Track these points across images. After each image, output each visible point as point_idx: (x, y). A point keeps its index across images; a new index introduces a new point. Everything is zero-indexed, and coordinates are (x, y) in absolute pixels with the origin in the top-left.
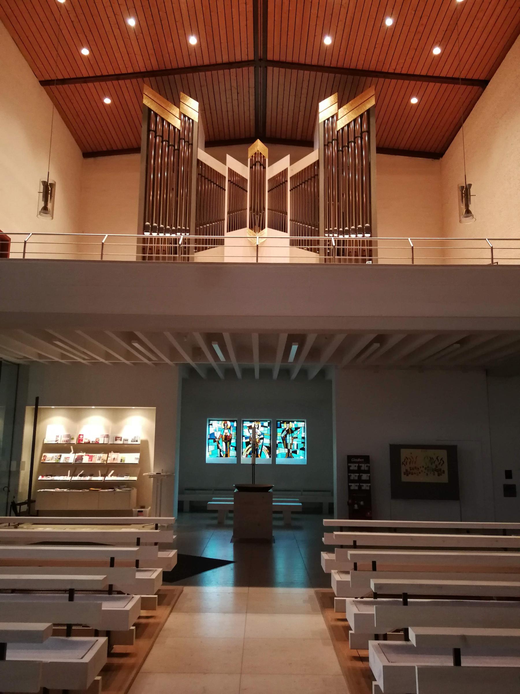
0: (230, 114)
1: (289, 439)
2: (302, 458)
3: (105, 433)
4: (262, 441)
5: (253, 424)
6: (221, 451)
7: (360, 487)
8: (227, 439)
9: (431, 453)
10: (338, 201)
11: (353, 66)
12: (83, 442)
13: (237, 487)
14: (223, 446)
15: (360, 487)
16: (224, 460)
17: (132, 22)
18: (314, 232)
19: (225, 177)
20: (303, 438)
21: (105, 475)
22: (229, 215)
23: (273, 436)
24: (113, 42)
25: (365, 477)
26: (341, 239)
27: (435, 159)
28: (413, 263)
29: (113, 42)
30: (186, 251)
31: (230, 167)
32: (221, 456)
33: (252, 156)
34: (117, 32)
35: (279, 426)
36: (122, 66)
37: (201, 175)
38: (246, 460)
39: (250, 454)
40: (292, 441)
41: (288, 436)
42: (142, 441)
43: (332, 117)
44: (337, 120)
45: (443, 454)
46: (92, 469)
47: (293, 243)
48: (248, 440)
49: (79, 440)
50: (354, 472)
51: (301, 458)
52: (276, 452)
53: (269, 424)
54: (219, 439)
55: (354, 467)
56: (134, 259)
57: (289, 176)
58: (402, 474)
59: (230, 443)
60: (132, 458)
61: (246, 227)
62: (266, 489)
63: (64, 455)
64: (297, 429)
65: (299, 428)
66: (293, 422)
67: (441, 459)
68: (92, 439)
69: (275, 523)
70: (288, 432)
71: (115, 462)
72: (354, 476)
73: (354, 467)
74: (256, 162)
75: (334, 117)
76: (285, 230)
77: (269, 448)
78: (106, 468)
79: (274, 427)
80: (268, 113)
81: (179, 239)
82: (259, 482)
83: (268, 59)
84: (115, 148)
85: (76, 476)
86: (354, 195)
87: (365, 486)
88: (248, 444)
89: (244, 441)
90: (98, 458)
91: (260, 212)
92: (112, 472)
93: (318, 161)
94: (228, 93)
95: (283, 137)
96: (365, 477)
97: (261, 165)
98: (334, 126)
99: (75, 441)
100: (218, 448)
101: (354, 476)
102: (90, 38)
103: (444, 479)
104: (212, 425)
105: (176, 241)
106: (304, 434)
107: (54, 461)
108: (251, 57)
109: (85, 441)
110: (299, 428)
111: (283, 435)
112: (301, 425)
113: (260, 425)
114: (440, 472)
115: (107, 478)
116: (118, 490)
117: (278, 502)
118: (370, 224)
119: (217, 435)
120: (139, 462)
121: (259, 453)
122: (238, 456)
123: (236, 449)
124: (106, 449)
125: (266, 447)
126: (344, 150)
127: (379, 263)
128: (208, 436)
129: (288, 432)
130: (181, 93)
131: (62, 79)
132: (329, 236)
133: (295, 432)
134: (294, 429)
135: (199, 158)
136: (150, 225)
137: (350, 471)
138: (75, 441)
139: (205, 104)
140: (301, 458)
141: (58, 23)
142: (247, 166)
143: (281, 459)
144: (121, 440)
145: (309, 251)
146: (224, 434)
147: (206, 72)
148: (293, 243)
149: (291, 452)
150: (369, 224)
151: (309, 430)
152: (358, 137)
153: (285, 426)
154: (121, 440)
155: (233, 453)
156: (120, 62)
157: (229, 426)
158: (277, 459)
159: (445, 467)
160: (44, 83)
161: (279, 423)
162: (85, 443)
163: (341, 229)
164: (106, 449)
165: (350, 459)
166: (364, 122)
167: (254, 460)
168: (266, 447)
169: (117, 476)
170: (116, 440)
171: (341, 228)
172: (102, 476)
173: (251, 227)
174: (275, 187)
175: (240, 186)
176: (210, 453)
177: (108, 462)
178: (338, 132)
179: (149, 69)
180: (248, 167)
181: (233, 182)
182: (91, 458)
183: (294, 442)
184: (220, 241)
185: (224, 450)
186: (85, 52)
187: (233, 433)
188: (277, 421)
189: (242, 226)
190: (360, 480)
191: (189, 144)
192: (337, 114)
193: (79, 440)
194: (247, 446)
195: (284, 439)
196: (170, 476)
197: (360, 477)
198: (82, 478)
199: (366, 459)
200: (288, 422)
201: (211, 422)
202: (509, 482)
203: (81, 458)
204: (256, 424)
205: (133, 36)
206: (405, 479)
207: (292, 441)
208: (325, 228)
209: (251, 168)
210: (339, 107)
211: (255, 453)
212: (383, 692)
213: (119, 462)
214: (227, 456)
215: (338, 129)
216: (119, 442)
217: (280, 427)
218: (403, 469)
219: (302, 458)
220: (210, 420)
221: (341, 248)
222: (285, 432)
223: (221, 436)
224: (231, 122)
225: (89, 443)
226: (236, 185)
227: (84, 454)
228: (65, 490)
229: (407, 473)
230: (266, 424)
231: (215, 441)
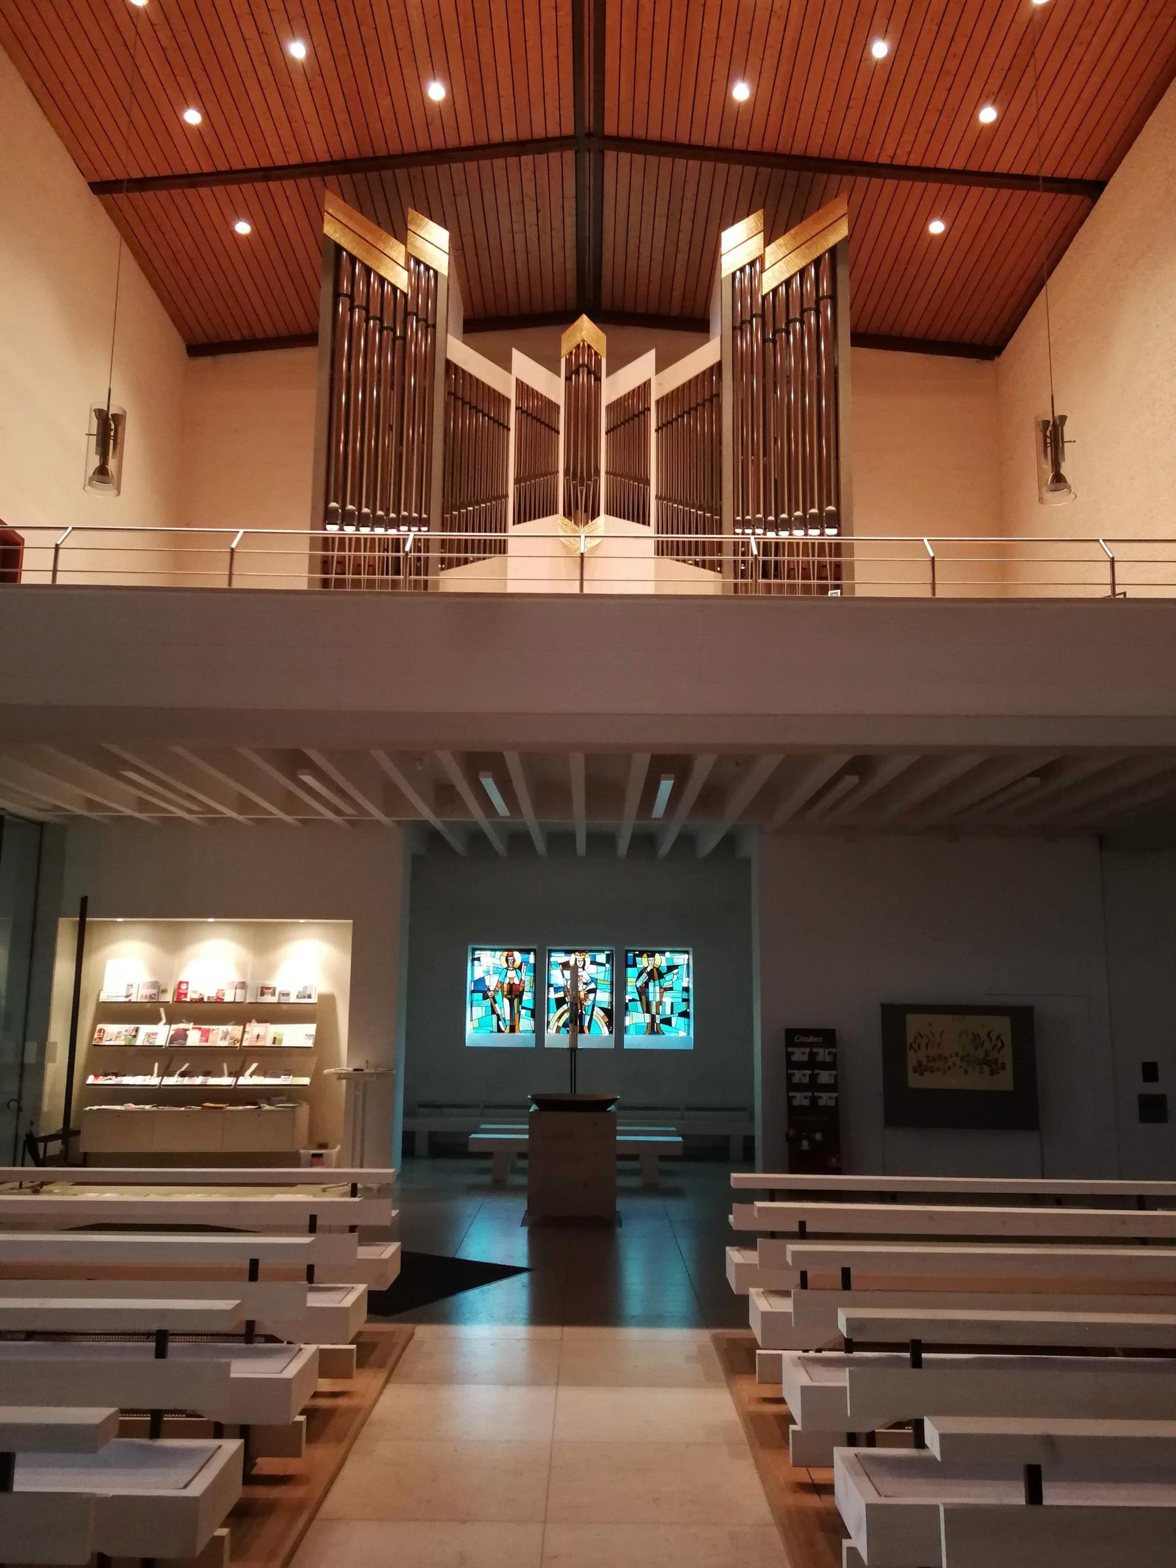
0: (521, 257)
1: (654, 991)
2: (682, 1034)
3: (237, 979)
4: (591, 996)
5: (571, 959)
6: (499, 1019)
7: (814, 1100)
8: (514, 993)
9: (975, 1023)
10: (765, 455)
11: (798, 149)
12: (188, 999)
13: (535, 1100)
14: (504, 1007)
15: (814, 1100)
16: (506, 1040)
17: (298, 50)
18: (710, 523)
19: (509, 401)
20: (686, 989)
21: (237, 1074)
22: (518, 486)
23: (618, 986)
24: (256, 95)
25: (824, 1077)
26: (771, 540)
27: (983, 359)
28: (934, 594)
29: (256, 95)
30: (422, 566)
31: (520, 378)
32: (499, 1030)
33: (571, 353)
34: (264, 71)
35: (630, 962)
36: (275, 150)
37: (455, 394)
38: (557, 1039)
39: (565, 1025)
40: (661, 997)
41: (651, 984)
42: (321, 997)
43: (752, 264)
44: (763, 270)
45: (1002, 1026)
46: (207, 1059)
47: (662, 549)
48: (561, 995)
49: (179, 994)
50: (800, 1066)
51: (680, 1034)
52: (623, 1021)
53: (609, 958)
54: (495, 991)
55: (799, 1055)
56: (303, 585)
57: (654, 397)
58: (910, 1071)
59: (520, 1002)
60: (297, 1035)
61: (556, 512)
62: (601, 1106)
63: (145, 1029)
64: (671, 968)
65: (676, 967)
66: (662, 953)
67: (998, 1037)
68: (209, 993)
69: (622, 1181)
70: (651, 975)
71: (259, 1044)
72: (802, 1076)
73: (799, 1055)
74: (579, 366)
76: (644, 520)
77: (608, 1012)
78: (239, 1058)
79: (620, 965)
80: (607, 254)
81: (405, 541)
82: (586, 1090)
83: (607, 133)
84: (260, 335)
85: (171, 1074)
86: (800, 442)
87: (825, 1099)
88: (560, 1002)
89: (553, 995)
90: (221, 1035)
91: (589, 479)
92: (254, 1066)
93: (719, 364)
94: (517, 209)
95: (641, 310)
96: (824, 1077)
97: (589, 373)
98: (755, 285)
99: (169, 997)
100: (493, 1011)
101: (802, 1076)
102: (204, 85)
103: (1005, 1081)
104: (478, 959)
105: (397, 544)
106: (687, 981)
107: (121, 1042)
108: (568, 129)
109: (191, 995)
111: (639, 984)
112: (681, 959)
113: (588, 960)
114: (995, 1067)
115: (243, 1081)
116: (267, 1107)
117: (629, 1135)
118: (838, 506)
119: (492, 982)
120: (315, 1043)
122: (539, 1031)
123: (533, 1016)
124: (240, 1014)
125: (602, 1009)
126: (777, 338)
127: (858, 594)
128: (470, 986)
129: (651, 975)
130: (410, 210)
131: (141, 179)
132: (743, 533)
133: (668, 977)
134: (664, 970)
135: (449, 357)
136: (340, 508)
137: (791, 1065)
138: (169, 997)
140: (680, 1034)
141: (132, 51)
142: (559, 375)
143: (636, 1038)
144: (273, 994)
145: (698, 566)
146: (507, 981)
147: (466, 164)
148: (662, 549)
149: (658, 1021)
150: (835, 507)
151: (699, 972)
152: (810, 309)
153: (643, 962)
154: (273, 994)
155: (526, 1023)
156: (272, 140)
157: (517, 963)
158: (625, 1036)
159: (1007, 1056)
160: (100, 188)
161: (630, 955)
162: (192, 1001)
164: (240, 1014)
165: (792, 1036)
166: (823, 276)
167: (574, 1040)
168: (602, 1009)
169: (265, 1075)
170: (262, 994)
171: (771, 515)
172: (230, 1075)
173: (568, 514)
174: (623, 423)
175: (542, 420)
176: (476, 1023)
177: (245, 1044)
178: (764, 298)
179: (338, 155)
180: (560, 376)
181: (526, 412)
182: (205, 1034)
183: (664, 1000)
184: (498, 543)
185: (508, 1017)
186: (193, 117)
187: (527, 977)
188: (628, 951)
189: (548, 510)
190: (813, 1085)
192: (761, 258)
193: (179, 994)
194: (558, 1007)
195: (643, 991)
196: (385, 1076)
197: (813, 1077)
198: (186, 1081)
199: (828, 1037)
200: (652, 954)
201: (477, 954)
202: (1152, 1089)
203: (183, 1035)
204: (580, 958)
205: (300, 82)
206: (915, 1081)
207: (661, 997)
208: (736, 514)
209: (568, 379)
211: (576, 1022)
212: (866, 1563)
213: (269, 1043)
214: (513, 1029)
215: (765, 291)
216: (268, 999)
217: (634, 965)
218: (912, 1059)
219: (682, 1034)
220: (474, 950)
221: (771, 561)
222: (644, 977)
223: (501, 984)
224: (522, 275)
225: (201, 1000)
226: (534, 418)
227: (191, 1025)
228: (147, 1107)
229: (920, 1069)
230: (601, 958)
231: (485, 997)
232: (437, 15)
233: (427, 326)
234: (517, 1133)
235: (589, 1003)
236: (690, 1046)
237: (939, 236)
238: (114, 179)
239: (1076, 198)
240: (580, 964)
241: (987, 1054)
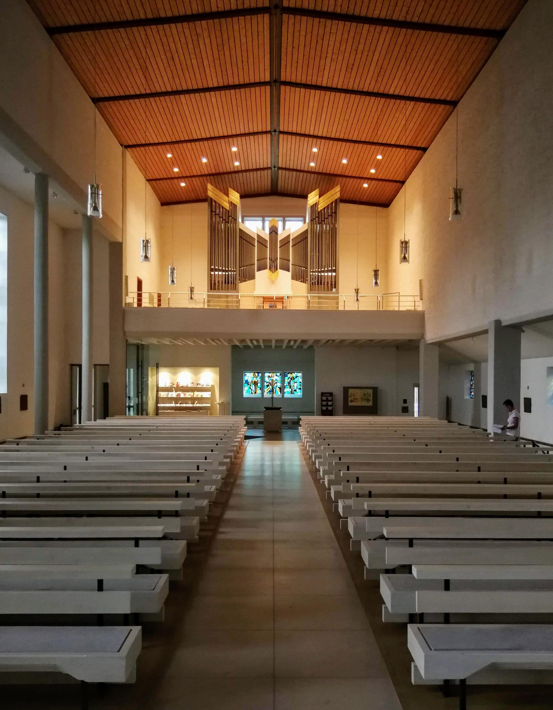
0: (256, 183)
1: (292, 382)
2: (299, 394)
3: (191, 382)
4: (276, 384)
6: (252, 390)
7: (327, 408)
8: (256, 383)
9: (365, 391)
10: (318, 253)
11: (328, 172)
12: (180, 386)
13: (264, 408)
14: (253, 387)
15: (327, 408)
16: (254, 396)
19: (255, 239)
20: (300, 382)
21: (193, 404)
23: (283, 381)
25: (330, 403)
27: (385, 207)
32: (252, 393)
35: (286, 375)
37: (241, 237)
38: (267, 395)
39: (269, 392)
40: (294, 384)
41: (291, 381)
42: (211, 385)
45: (371, 391)
46: (185, 400)
48: (268, 384)
49: (178, 385)
50: (324, 401)
51: (299, 394)
52: (284, 390)
53: (280, 374)
54: (251, 383)
55: (324, 398)
57: (291, 238)
58: (349, 401)
59: (257, 386)
60: (207, 395)
63: (170, 393)
64: (296, 377)
65: (298, 377)
66: (294, 373)
67: (369, 394)
68: (185, 385)
69: (283, 427)
71: (198, 397)
72: (324, 403)
73: (324, 398)
74: (272, 231)
76: (289, 271)
77: (280, 388)
78: (193, 400)
79: (283, 376)
82: (276, 405)
83: (282, 80)
84: (181, 200)
85: (178, 404)
87: (330, 408)
88: (268, 386)
89: (266, 384)
90: (188, 395)
92: (196, 402)
93: (307, 229)
95: (289, 193)
96: (330, 403)
99: (175, 386)
100: (250, 388)
101: (324, 403)
103: (370, 404)
104: (246, 375)
106: (301, 380)
107: (165, 396)
108: (268, 79)
110: (298, 377)
111: (289, 381)
112: (300, 375)
113: (275, 375)
114: (368, 400)
115: (194, 405)
116: (201, 411)
117: (284, 417)
118: (336, 267)
119: (250, 381)
120: (211, 396)
122: (263, 394)
123: (261, 389)
124: (193, 390)
125: (279, 388)
128: (244, 382)
129: (291, 379)
130: (229, 188)
133: (296, 379)
134: (295, 377)
135: (240, 227)
137: (322, 401)
138: (175, 386)
140: (299, 394)
143: (287, 395)
144: (200, 385)
146: (254, 381)
147: (221, 19)
149: (293, 391)
151: (304, 378)
153: (289, 375)
154: (200, 385)
155: (259, 391)
157: (256, 376)
158: (285, 394)
159: (371, 398)
160: (148, 180)
161: (286, 373)
162: (181, 387)
163: (320, 270)
164: (193, 390)
165: (323, 394)
167: (273, 395)
168: (279, 388)
169: (199, 404)
170: (197, 385)
172: (191, 404)
176: (246, 391)
177: (194, 397)
182: (185, 394)
183: (295, 385)
185: (254, 390)
187: (259, 379)
188: (285, 373)
189: (265, 268)
190: (327, 405)
191: (234, 220)
193: (178, 385)
194: (267, 387)
195: (289, 383)
196: (229, 403)
197: (327, 403)
198: (182, 405)
199: (331, 394)
200: (292, 373)
201: (246, 374)
202: (405, 405)
203: (179, 395)
204: (273, 374)
206: (350, 404)
207: (294, 384)
210: (320, 197)
211: (272, 391)
212: (333, 499)
213: (200, 397)
214: (255, 393)
216: (199, 386)
217: (287, 376)
218: (350, 399)
219: (299, 394)
220: (245, 372)
222: (290, 379)
223: (252, 381)
225: (183, 387)
227: (181, 392)
228: (173, 411)
229: (351, 401)
230: (278, 374)
231: (248, 385)
232: (220, 51)
234: (261, 417)
235: (275, 386)
237: (372, 169)
238: (103, 96)
240: (273, 376)
241: (367, 398)
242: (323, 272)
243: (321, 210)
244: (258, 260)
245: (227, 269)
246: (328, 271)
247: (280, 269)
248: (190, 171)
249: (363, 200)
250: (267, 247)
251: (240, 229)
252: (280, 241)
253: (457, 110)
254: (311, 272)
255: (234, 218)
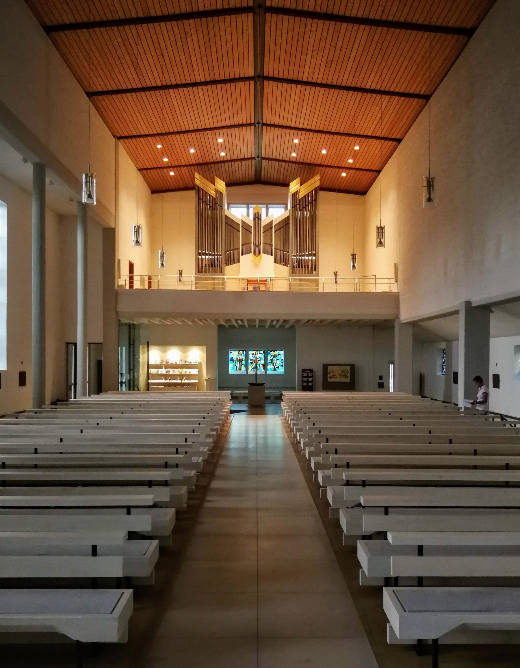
0: (240, 172)
1: (275, 360)
2: (282, 370)
3: (180, 359)
4: (259, 361)
5: (254, 352)
6: (237, 367)
7: (308, 384)
8: (240, 361)
9: (343, 368)
10: (299, 238)
11: (308, 162)
12: (169, 363)
13: (249, 384)
14: (238, 364)
15: (308, 384)
16: (239, 372)
19: (240, 225)
20: (283, 360)
21: (182, 380)
23: (266, 359)
25: (310, 379)
27: (362, 195)
32: (237, 370)
35: (269, 353)
37: (227, 223)
38: (251, 371)
39: (253, 369)
40: (276, 361)
41: (274, 358)
42: (199, 363)
45: (348, 368)
46: (174, 376)
48: (252, 361)
49: (167, 362)
50: (305, 377)
51: (281, 370)
52: (267, 367)
53: (264, 352)
54: (236, 360)
55: (305, 375)
57: (274, 224)
58: (328, 378)
59: (242, 363)
60: (194, 371)
62: (262, 384)
63: (160, 370)
64: (279, 355)
65: (280, 354)
66: (277, 351)
67: (347, 371)
68: (174, 362)
69: (266, 402)
70: (274, 356)
71: (186, 373)
72: (305, 379)
73: (305, 375)
74: (256, 217)
75: (297, 192)
76: (272, 255)
77: (263, 365)
78: (181, 376)
79: (267, 354)
82: (259, 381)
83: (265, 75)
84: (170, 188)
85: (167, 380)
87: (310, 384)
88: (252, 363)
89: (250, 361)
90: (177, 371)
92: (185, 378)
93: (289, 216)
95: (272, 181)
96: (310, 379)
99: (165, 363)
100: (235, 365)
101: (305, 379)
103: (348, 380)
104: (231, 353)
106: (283, 358)
107: (155, 373)
108: (252, 74)
109: (170, 362)
110: (280, 354)
112: (282, 352)
113: (258, 353)
114: (346, 377)
115: (183, 381)
116: (189, 387)
117: (267, 393)
118: (316, 252)
119: (235, 358)
120: (198, 373)
121: (258, 368)
122: (247, 370)
123: (245, 366)
124: (181, 367)
125: (262, 365)
128: (230, 359)
129: (274, 356)
130: (216, 177)
133: (278, 357)
134: (277, 355)
135: (226, 214)
137: (303, 377)
138: (165, 363)
139: (212, 70)
140: (281, 370)
143: (270, 372)
144: (188, 362)
146: (239, 358)
147: (207, 18)
149: (276, 367)
151: (285, 355)
153: (272, 353)
154: (188, 362)
155: (243, 368)
157: (241, 354)
158: (268, 371)
159: (349, 374)
160: (139, 170)
161: (269, 351)
162: (170, 364)
163: (301, 254)
164: (181, 367)
165: (303, 371)
167: (256, 372)
168: (262, 365)
169: (187, 380)
170: (186, 362)
172: (180, 380)
176: (231, 368)
177: (183, 373)
182: (174, 371)
183: (277, 362)
185: (239, 367)
187: (243, 357)
188: (268, 351)
189: (249, 252)
190: (308, 381)
193: (167, 362)
194: (251, 364)
195: (272, 360)
196: (215, 379)
197: (308, 380)
198: (171, 381)
199: (311, 371)
200: (274, 351)
201: (231, 352)
202: (381, 381)
203: (169, 371)
204: (256, 352)
206: (329, 380)
207: (276, 361)
211: (256, 368)
212: (314, 470)
213: (188, 373)
214: (240, 370)
216: (187, 363)
217: (270, 354)
218: (329, 375)
219: (282, 370)
220: (230, 350)
222: (272, 357)
223: (237, 359)
225: (172, 364)
227: (170, 369)
228: (163, 387)
229: (330, 377)
230: (262, 352)
231: (233, 362)
233: (220, 207)
236: (204, 348)
238: (97, 91)
239: (421, 100)
242: (304, 256)
243: (302, 198)
244: (242, 245)
245: (213, 253)
246: (308, 255)
247: (263, 253)
248: (179, 160)
249: (342, 189)
250: (251, 233)
251: (225, 215)
252: (263, 227)
253: (430, 103)
254: (292, 256)
255: (220, 205)
